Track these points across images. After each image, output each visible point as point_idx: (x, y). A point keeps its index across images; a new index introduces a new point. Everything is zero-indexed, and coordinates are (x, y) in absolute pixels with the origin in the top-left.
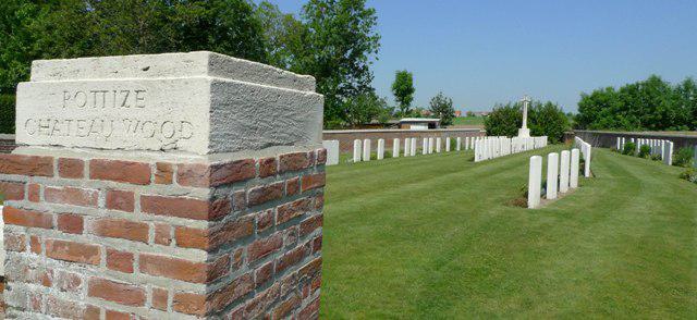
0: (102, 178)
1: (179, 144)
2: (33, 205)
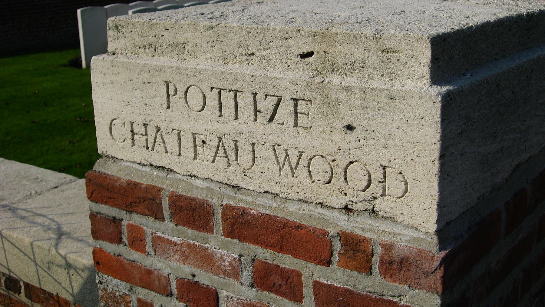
0: (243, 239)
1: (379, 204)
2: (135, 255)
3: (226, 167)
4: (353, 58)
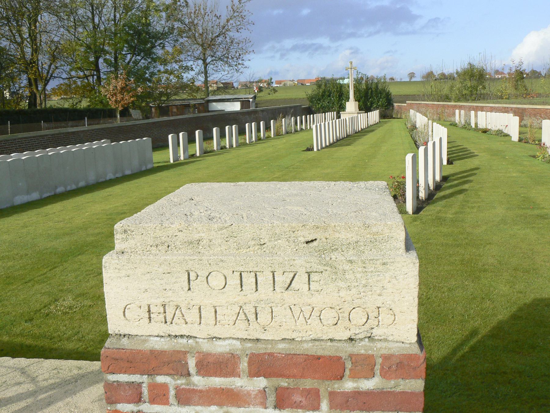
3: (247, 327)
4: (348, 241)
